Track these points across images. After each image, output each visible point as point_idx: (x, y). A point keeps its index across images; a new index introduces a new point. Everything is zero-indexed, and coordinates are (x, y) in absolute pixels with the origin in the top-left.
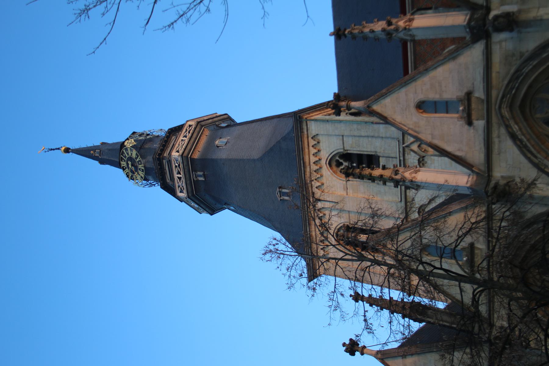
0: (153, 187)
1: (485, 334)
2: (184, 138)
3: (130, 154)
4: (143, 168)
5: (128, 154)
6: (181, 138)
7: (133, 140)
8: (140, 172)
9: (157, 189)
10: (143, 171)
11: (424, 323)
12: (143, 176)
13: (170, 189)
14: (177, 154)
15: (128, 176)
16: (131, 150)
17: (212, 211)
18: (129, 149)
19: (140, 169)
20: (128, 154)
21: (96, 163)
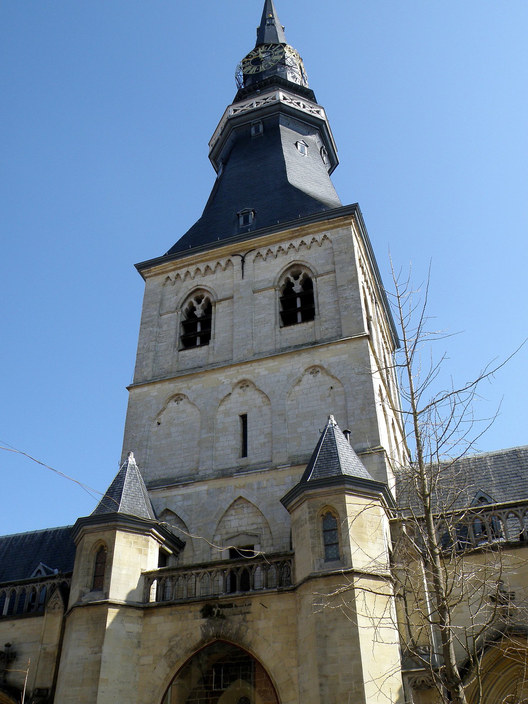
0: (245, 56)
1: (440, 554)
2: (302, 106)
3: (275, 53)
4: (260, 71)
5: (275, 51)
6: (302, 103)
8: (255, 68)
9: (235, 91)
10: (256, 71)
11: (155, 581)
12: (251, 73)
13: (240, 97)
14: (282, 98)
15: (247, 57)
17: (214, 157)
18: (282, 50)
19: (259, 67)
20: (275, 51)
21: (258, 25)
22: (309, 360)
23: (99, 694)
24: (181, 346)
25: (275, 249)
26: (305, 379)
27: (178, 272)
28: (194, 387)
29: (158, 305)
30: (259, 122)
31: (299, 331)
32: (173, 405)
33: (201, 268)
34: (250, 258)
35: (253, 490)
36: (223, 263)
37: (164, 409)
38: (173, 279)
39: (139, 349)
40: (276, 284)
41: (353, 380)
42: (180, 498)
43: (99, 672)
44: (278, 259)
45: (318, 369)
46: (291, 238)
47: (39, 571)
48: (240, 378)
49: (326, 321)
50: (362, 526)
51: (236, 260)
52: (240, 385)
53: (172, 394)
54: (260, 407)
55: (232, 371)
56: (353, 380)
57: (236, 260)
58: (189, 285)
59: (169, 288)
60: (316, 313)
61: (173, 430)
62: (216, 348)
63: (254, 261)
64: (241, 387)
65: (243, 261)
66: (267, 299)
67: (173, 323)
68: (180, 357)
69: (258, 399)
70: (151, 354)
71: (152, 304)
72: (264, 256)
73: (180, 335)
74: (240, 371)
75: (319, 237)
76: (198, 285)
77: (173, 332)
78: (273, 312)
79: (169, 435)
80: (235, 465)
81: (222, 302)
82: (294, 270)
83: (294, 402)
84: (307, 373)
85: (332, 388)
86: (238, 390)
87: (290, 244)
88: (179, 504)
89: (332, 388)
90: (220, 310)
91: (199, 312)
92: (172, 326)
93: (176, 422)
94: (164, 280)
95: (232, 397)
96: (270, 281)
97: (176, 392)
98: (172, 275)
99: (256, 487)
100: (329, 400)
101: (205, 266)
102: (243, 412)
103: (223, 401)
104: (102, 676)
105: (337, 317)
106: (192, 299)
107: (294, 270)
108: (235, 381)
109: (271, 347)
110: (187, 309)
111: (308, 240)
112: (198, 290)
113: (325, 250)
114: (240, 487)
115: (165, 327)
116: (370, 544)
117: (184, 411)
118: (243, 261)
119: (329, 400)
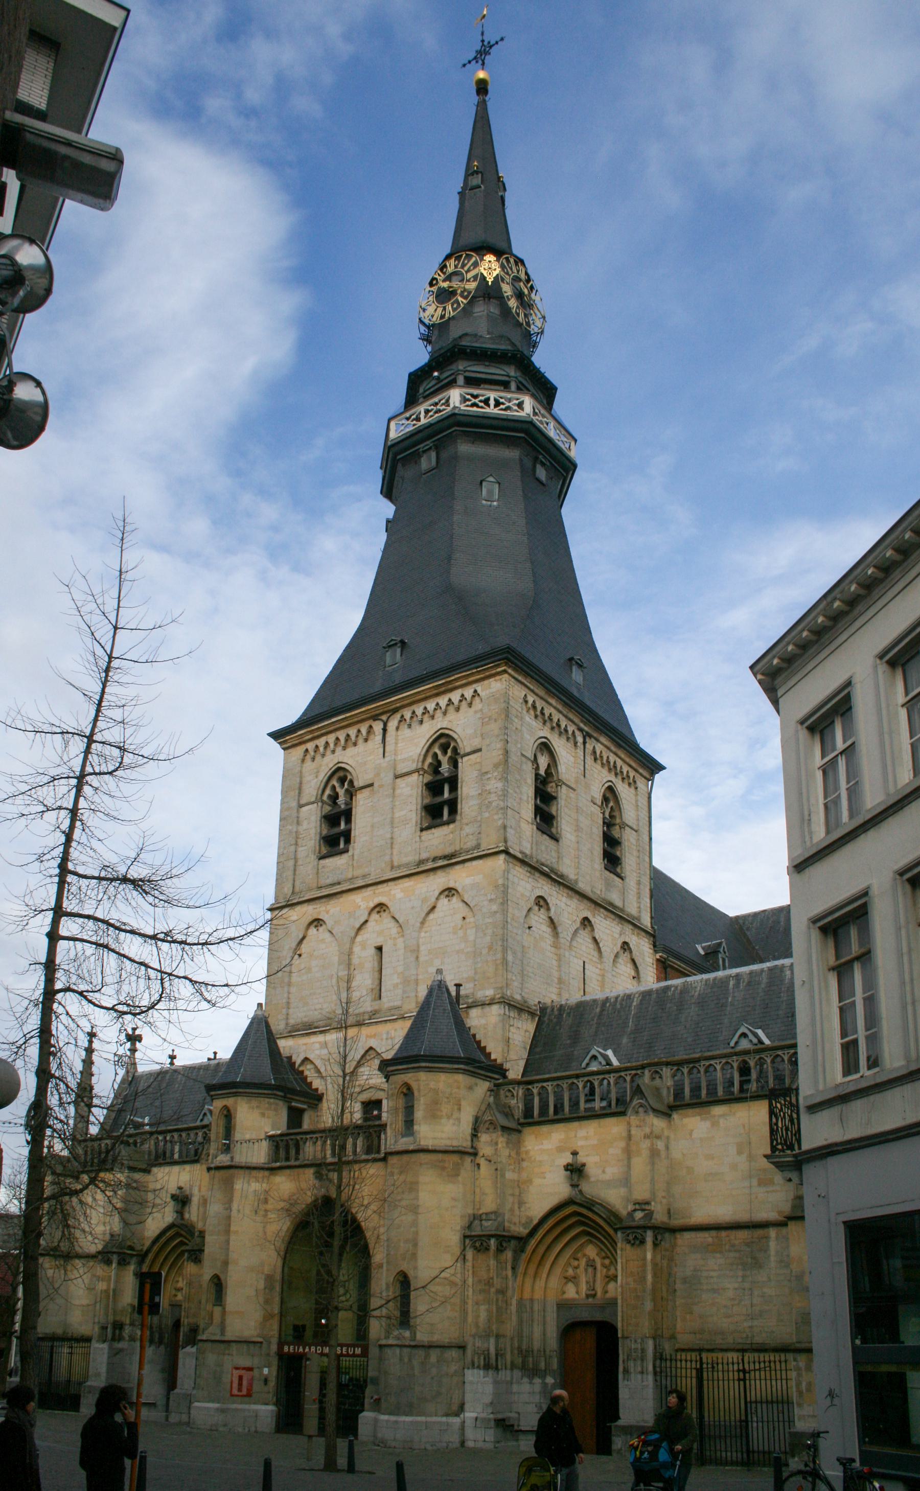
7: (498, 271)
10: (442, 317)
16: (475, 278)
19: (444, 309)
22: (443, 880)
23: (231, 1243)
24: (324, 851)
25: (419, 710)
26: (439, 905)
27: (317, 742)
28: (332, 911)
29: (297, 792)
30: (430, 448)
31: (440, 839)
32: (312, 931)
33: (453, 700)
34: (393, 724)
35: (382, 1039)
36: (364, 731)
37: (304, 938)
38: (312, 754)
39: (279, 856)
40: (420, 765)
41: (484, 910)
42: (317, 1046)
43: (230, 1225)
44: (424, 725)
45: (453, 892)
46: (437, 695)
47: (205, 1114)
48: (377, 901)
49: (467, 824)
50: (437, 1103)
51: (378, 726)
52: (377, 909)
53: (310, 919)
54: (395, 938)
55: (368, 892)
56: (484, 910)
57: (378, 726)
58: (328, 763)
59: (309, 765)
60: (459, 811)
61: (314, 963)
62: (356, 857)
63: (397, 728)
64: (379, 912)
65: (385, 730)
66: (409, 788)
67: (313, 818)
68: (320, 867)
69: (394, 929)
70: (291, 863)
71: (292, 787)
72: (408, 720)
73: (321, 834)
74: (377, 892)
75: (468, 692)
76: (339, 763)
77: (313, 832)
78: (414, 808)
79: (309, 970)
80: (369, 1009)
81: (363, 790)
82: (443, 741)
83: (428, 934)
84: (442, 896)
85: (464, 918)
86: (375, 916)
87: (473, 690)
88: (317, 1052)
89: (464, 918)
90: (361, 803)
91: (445, 768)
92: (311, 822)
93: (316, 953)
94: (302, 754)
95: (369, 924)
96: (413, 761)
97: (316, 916)
98: (310, 746)
99: (384, 1036)
100: (461, 933)
101: (334, 739)
102: (379, 944)
103: (360, 929)
104: (232, 1228)
105: (479, 818)
106: (436, 750)
107: (443, 741)
108: (372, 905)
109: (412, 858)
110: (431, 764)
111: (455, 696)
112: (442, 735)
113: (476, 712)
114: (371, 1037)
115: (305, 825)
116: (444, 1121)
117: (323, 941)
118: (385, 730)
119: (461, 933)
